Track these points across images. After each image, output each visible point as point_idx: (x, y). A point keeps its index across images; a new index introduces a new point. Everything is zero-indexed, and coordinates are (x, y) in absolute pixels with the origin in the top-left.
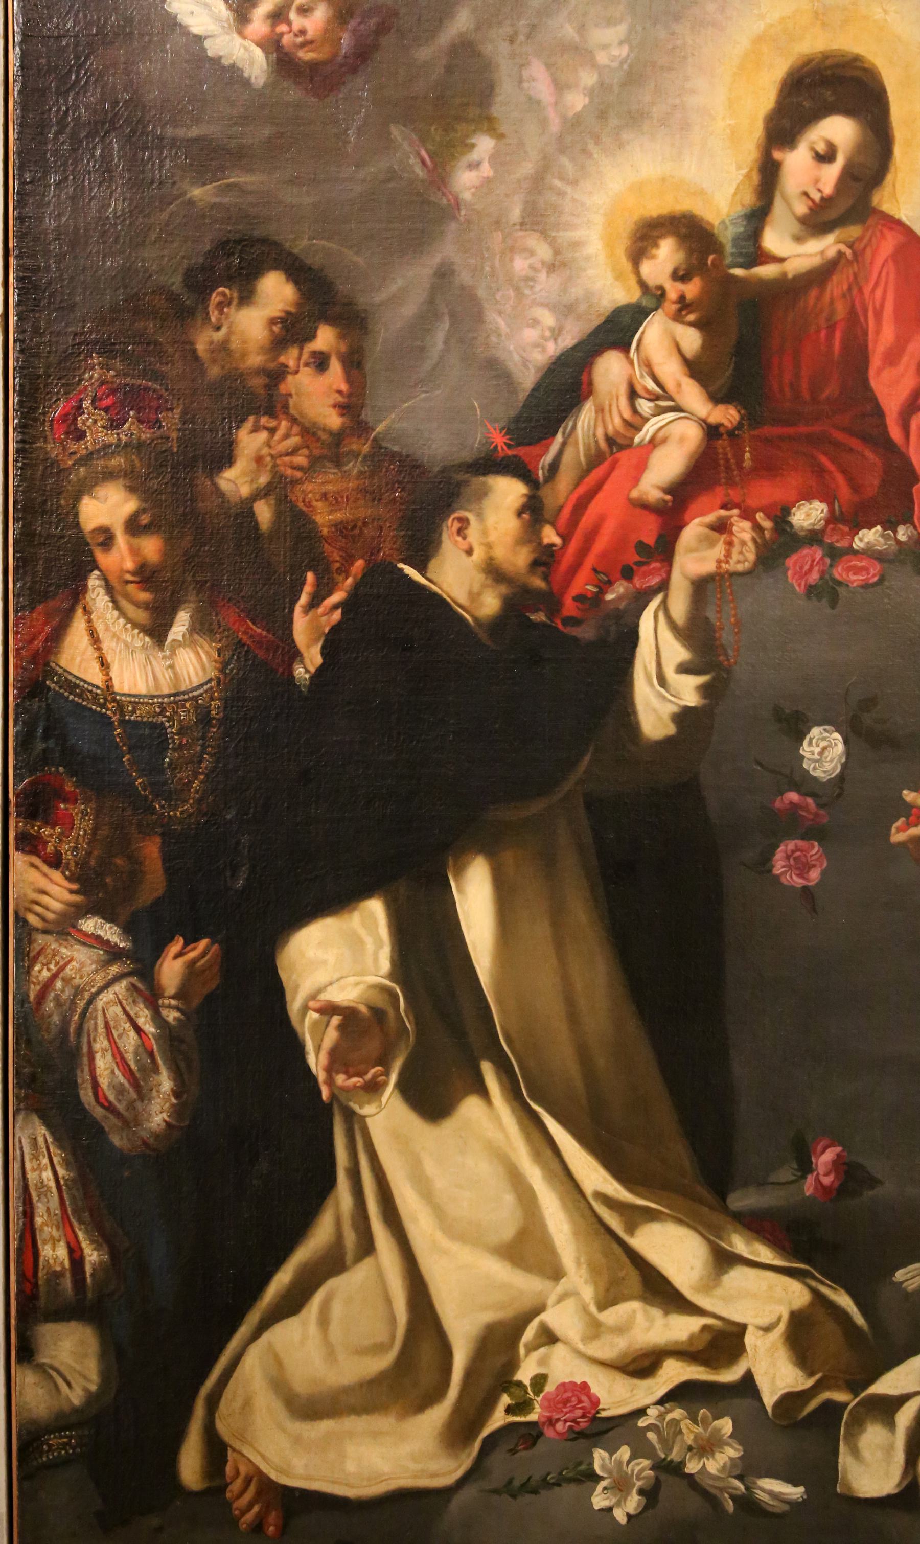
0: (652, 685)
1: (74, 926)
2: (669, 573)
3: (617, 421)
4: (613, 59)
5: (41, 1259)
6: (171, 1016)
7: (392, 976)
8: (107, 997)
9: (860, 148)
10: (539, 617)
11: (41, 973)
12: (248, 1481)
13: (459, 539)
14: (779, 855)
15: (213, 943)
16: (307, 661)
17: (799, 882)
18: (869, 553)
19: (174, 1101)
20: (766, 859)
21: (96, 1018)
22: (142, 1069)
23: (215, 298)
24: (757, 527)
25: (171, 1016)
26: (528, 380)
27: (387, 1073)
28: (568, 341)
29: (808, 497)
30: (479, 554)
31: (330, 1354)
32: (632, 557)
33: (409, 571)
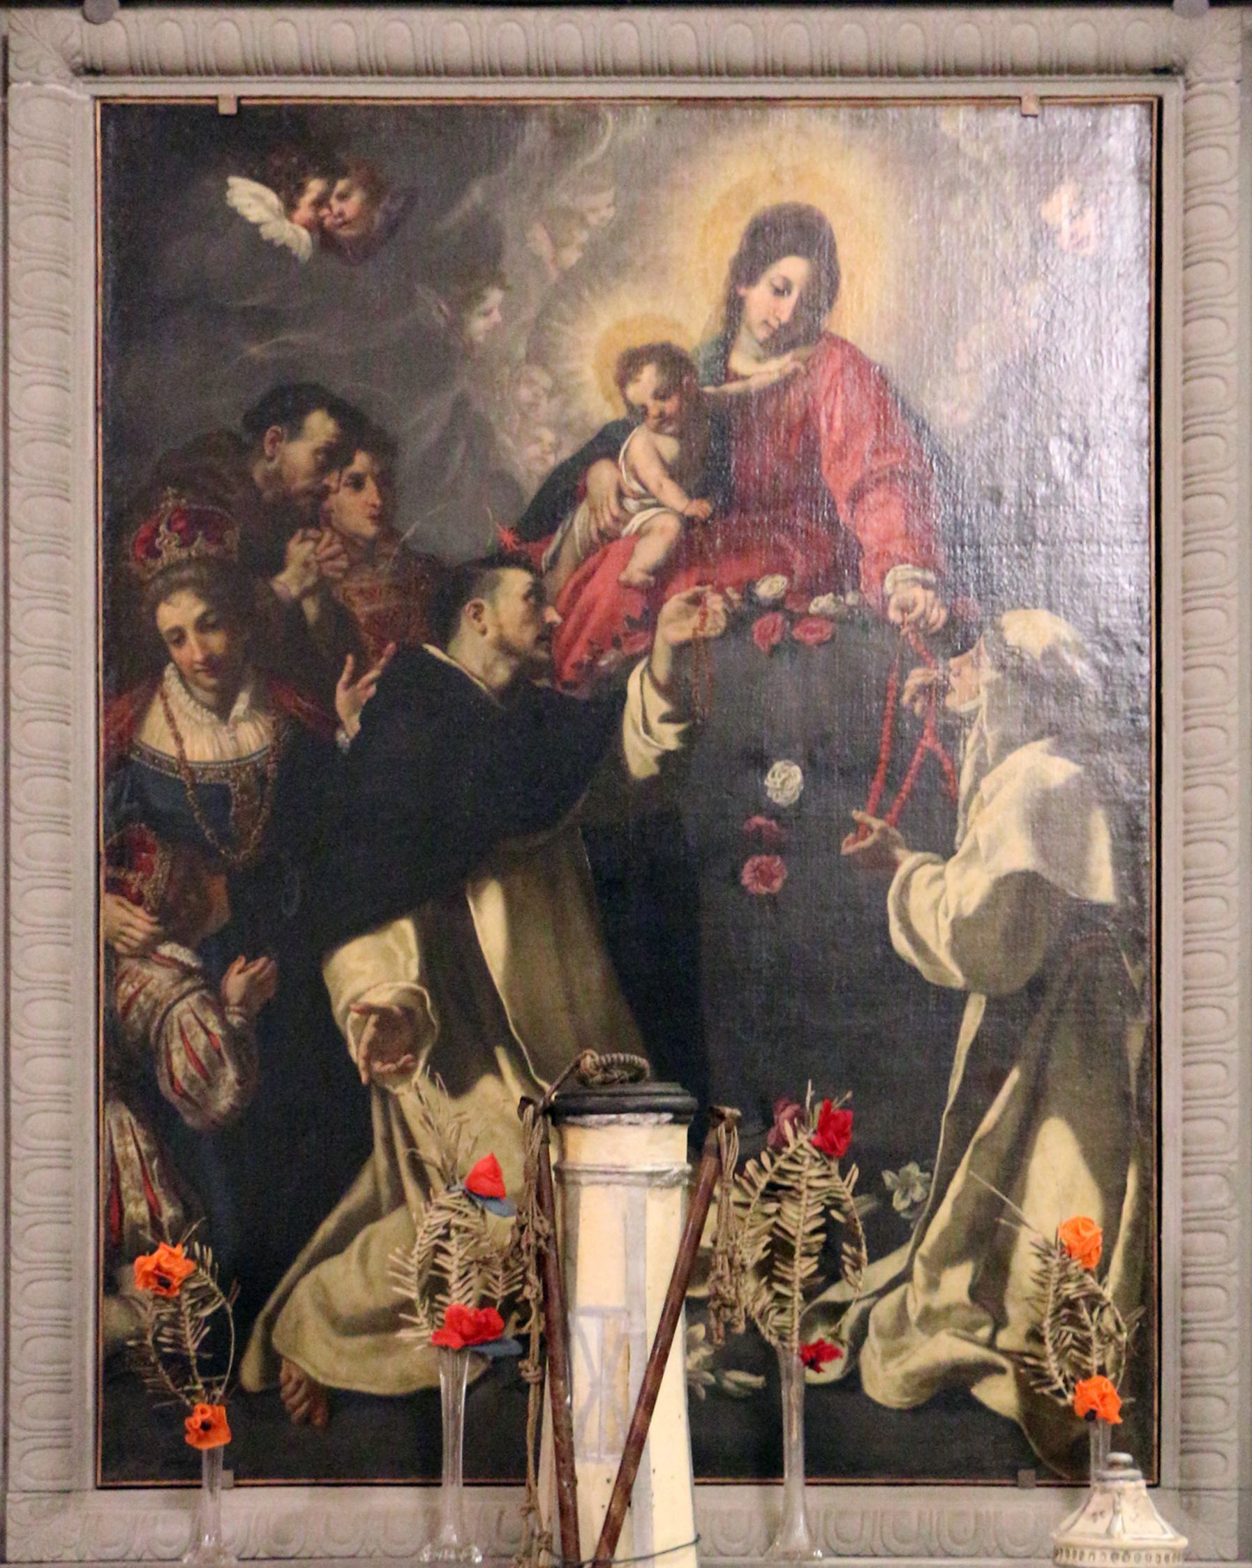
0: (638, 734)
1: (155, 952)
2: (653, 642)
3: (608, 518)
4: (602, 220)
5: (126, 1216)
6: (235, 1020)
7: (420, 981)
8: (182, 1006)
10: (543, 683)
11: (127, 989)
12: (299, 1384)
13: (475, 622)
14: (748, 866)
15: (270, 960)
16: (348, 729)
17: (764, 890)
19: (237, 1088)
20: (735, 875)
21: (172, 1024)
22: (211, 1063)
23: (269, 435)
24: (727, 600)
25: (235, 1020)
26: (532, 487)
27: (416, 1059)
28: (566, 453)
29: (771, 571)
30: (492, 633)
31: (369, 1283)
33: (432, 650)
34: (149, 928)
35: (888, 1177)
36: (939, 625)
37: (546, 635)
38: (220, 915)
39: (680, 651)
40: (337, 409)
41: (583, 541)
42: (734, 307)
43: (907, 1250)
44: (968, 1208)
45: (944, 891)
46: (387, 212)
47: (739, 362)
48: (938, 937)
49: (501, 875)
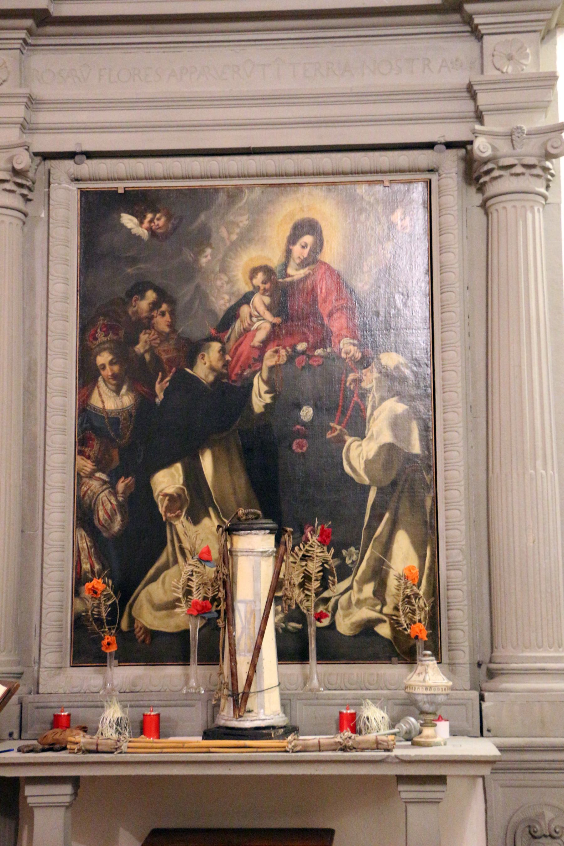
1: (94, 475)
2: (262, 366)
3: (247, 324)
7: (183, 485)
9: (315, 243)
10: (225, 381)
11: (84, 488)
12: (141, 628)
14: (295, 443)
17: (300, 451)
18: (319, 356)
20: (290, 446)
23: (134, 299)
24: (287, 351)
25: (121, 499)
26: (221, 314)
27: (182, 512)
28: (233, 303)
29: (301, 341)
30: (208, 364)
31: (165, 592)
32: (252, 361)
33: (188, 370)
34: (92, 467)
35: (344, 552)
36: (359, 358)
37: (226, 364)
38: (116, 462)
39: (271, 369)
40: (157, 290)
41: (238, 332)
42: (288, 252)
43: (351, 578)
44: (372, 563)
45: (362, 450)
46: (173, 224)
47: (290, 271)
48: (360, 466)
49: (211, 447)
